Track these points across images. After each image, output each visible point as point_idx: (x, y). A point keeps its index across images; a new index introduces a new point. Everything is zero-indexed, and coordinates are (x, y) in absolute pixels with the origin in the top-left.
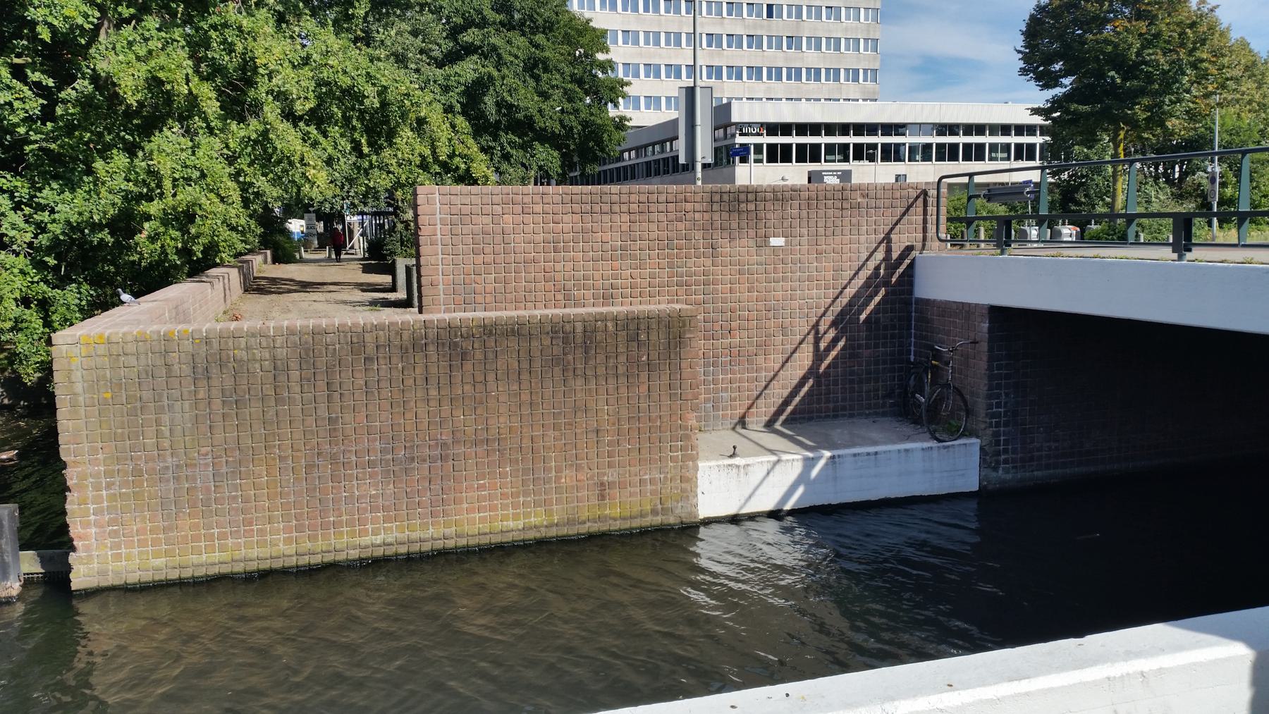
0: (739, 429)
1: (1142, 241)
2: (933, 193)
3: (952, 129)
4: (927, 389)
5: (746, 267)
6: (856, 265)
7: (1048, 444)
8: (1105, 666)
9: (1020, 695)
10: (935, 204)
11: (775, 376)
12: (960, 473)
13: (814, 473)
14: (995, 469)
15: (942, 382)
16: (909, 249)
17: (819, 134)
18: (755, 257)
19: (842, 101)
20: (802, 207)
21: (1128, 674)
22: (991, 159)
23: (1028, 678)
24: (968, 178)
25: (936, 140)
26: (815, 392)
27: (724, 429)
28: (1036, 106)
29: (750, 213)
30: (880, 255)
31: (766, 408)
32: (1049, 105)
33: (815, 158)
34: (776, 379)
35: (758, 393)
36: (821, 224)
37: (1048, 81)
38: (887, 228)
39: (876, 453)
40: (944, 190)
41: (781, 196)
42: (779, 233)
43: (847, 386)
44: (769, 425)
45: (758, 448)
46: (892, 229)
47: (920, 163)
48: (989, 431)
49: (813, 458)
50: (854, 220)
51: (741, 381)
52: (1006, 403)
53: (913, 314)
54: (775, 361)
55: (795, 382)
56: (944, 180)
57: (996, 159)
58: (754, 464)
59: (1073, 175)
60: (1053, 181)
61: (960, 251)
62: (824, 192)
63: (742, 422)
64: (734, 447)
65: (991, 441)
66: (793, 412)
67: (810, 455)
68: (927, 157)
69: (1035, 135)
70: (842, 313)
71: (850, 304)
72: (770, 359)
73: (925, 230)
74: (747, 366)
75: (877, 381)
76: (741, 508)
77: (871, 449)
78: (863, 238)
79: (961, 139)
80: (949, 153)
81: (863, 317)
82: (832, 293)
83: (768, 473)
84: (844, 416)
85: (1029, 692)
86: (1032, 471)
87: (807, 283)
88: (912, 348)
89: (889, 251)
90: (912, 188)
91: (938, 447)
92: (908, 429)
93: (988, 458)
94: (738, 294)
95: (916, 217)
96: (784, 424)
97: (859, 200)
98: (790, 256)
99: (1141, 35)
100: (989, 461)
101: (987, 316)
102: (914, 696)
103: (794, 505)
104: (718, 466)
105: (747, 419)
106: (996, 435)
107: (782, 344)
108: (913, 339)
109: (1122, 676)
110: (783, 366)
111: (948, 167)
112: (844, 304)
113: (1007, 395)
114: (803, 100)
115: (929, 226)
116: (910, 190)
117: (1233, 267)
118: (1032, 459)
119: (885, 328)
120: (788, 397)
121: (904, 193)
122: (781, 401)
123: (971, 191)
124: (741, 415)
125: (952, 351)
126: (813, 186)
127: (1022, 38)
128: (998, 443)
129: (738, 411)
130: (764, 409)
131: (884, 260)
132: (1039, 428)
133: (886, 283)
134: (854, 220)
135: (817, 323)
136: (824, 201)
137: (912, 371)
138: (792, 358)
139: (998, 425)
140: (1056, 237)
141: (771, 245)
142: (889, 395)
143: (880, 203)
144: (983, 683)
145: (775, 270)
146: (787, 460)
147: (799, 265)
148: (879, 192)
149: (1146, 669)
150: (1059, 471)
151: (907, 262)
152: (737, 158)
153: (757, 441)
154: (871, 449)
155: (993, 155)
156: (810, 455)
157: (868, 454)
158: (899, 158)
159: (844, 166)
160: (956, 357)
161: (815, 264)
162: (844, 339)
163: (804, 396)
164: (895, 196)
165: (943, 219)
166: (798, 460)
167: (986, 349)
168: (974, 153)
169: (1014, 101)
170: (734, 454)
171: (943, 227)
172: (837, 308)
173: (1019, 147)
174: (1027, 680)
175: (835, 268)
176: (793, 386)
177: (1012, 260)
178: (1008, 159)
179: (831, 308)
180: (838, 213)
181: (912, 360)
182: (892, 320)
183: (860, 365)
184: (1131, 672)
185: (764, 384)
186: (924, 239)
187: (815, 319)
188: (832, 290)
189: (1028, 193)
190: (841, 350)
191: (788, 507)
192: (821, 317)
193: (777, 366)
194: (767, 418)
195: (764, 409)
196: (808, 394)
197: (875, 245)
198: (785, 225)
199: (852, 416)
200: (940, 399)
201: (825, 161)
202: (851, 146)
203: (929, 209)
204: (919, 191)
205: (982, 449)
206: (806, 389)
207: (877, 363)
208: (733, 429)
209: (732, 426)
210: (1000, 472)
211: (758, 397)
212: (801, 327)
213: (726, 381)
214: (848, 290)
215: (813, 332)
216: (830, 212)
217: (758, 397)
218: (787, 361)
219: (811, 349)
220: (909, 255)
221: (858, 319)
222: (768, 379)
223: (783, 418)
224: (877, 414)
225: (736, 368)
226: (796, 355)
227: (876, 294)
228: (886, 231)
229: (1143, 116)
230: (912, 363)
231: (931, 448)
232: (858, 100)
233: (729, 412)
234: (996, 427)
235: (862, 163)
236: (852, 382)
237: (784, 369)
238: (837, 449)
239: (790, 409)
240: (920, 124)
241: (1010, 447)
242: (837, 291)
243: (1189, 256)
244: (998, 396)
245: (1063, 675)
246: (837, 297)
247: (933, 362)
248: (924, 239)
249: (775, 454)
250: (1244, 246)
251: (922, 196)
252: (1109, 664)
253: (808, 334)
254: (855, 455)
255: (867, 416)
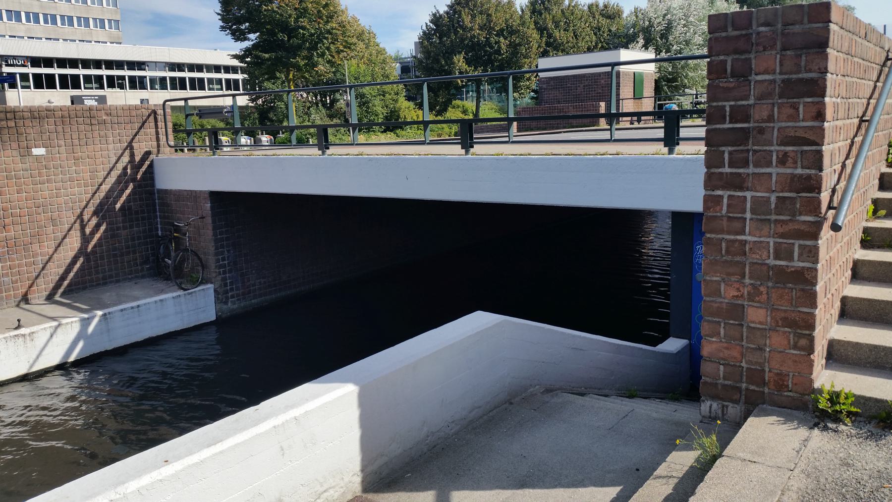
0: (23, 305)
1: (311, 143)
2: (160, 112)
3: (179, 67)
4: (173, 254)
5: (13, 173)
6: (108, 167)
7: (259, 281)
8: (272, 419)
9: (216, 454)
10: (163, 120)
11: (50, 259)
12: (202, 309)
13: (91, 329)
14: (226, 303)
15: (182, 247)
16: (148, 153)
17: (52, 67)
18: (20, 165)
19: (93, 43)
20: (58, 124)
21: (287, 421)
22: (210, 89)
23: (221, 441)
24: (183, 101)
25: (169, 74)
26: (86, 267)
27: (8, 307)
28: (234, 53)
29: (11, 129)
30: (126, 159)
31: (45, 285)
32: (243, 53)
33: (76, 86)
34: (52, 260)
35: (37, 274)
36: (75, 136)
37: (239, 36)
38: (129, 139)
39: (138, 306)
40: (168, 110)
41: (37, 115)
42: (39, 144)
43: (112, 259)
44: (50, 298)
45: (41, 318)
46: (133, 139)
47: (159, 91)
48: (219, 278)
49: (88, 318)
50: (102, 133)
51: (19, 266)
52: (228, 257)
53: (157, 201)
54: (48, 247)
55: (68, 261)
56: (167, 103)
57: (213, 89)
58: (37, 332)
59: (265, 101)
60: (252, 105)
61: (193, 154)
62: (74, 112)
63: (25, 299)
64: (19, 321)
65: (221, 284)
66: (69, 285)
67: (86, 316)
68: (163, 87)
69: (238, 73)
70: (101, 205)
71: (107, 197)
72: (44, 246)
73: (158, 139)
74: (24, 253)
75: (134, 252)
76: (31, 367)
77: (135, 304)
78: (111, 146)
79: (187, 75)
80: (180, 84)
81: (118, 206)
82: (91, 190)
83: (52, 336)
84: (111, 282)
85: (223, 450)
86: (251, 300)
87: (69, 183)
88: (159, 226)
89: (132, 155)
90: (145, 108)
91: (185, 294)
92: (161, 285)
93: (220, 296)
94: (8, 196)
95: (150, 129)
96: (63, 295)
97: (104, 118)
98: (52, 162)
99: (296, 9)
100: (221, 298)
101: (209, 198)
102: (140, 476)
103: (77, 357)
104: (4, 338)
105: (29, 296)
106: (224, 279)
107: (52, 235)
108: (159, 219)
109: (283, 423)
110: (56, 250)
111: (169, 94)
112: (101, 197)
113: (228, 251)
114: (61, 41)
115: (161, 136)
116: (143, 110)
117: (352, 158)
118: (249, 292)
119: (137, 213)
120: (63, 274)
121: (139, 112)
122: (57, 278)
123: (187, 111)
124: (23, 293)
125: (187, 225)
126: (78, 107)
127: (220, 5)
128: (226, 285)
129: (20, 291)
130: (44, 286)
131: (129, 162)
132: (252, 271)
133: (134, 180)
134: (102, 133)
135: (81, 214)
136: (76, 119)
137: (161, 242)
138: (64, 243)
139: (225, 272)
140: (257, 143)
141: (34, 154)
142: (146, 262)
143: (121, 120)
144: (190, 453)
145: (40, 175)
146: (67, 323)
147: (60, 169)
148: (119, 111)
149: (297, 415)
150: (268, 297)
151: (147, 163)
152: (6, 85)
153: (24, 311)
154: (135, 304)
155: (211, 86)
156: (86, 316)
157: (132, 308)
158: (143, 87)
159: (100, 92)
160: (191, 229)
161: (74, 168)
162: (105, 224)
163: (77, 272)
164: (132, 115)
165: (170, 131)
166: (76, 322)
167: (210, 221)
168: (197, 84)
169: (221, 49)
170: (19, 326)
171: (171, 137)
172: (97, 200)
173: (228, 81)
174: (220, 443)
175: (91, 170)
176: (67, 264)
177: (220, 159)
178: (222, 89)
179: (92, 201)
180: (89, 128)
181: (160, 235)
182: (141, 207)
183: (120, 242)
184: (288, 419)
185: (41, 266)
186: (158, 146)
187: (79, 211)
188: (90, 187)
189: (226, 112)
190: (104, 232)
191: (72, 359)
192: (84, 208)
193: (51, 251)
194: (47, 293)
195: (44, 286)
196: (80, 269)
197: (121, 152)
198: (44, 137)
199: (118, 281)
200: (182, 261)
201: (85, 88)
202: (105, 78)
203: (159, 124)
204: (150, 111)
205: (215, 291)
206: (78, 265)
207: (133, 239)
208: (18, 306)
209: (16, 303)
210: (229, 304)
211: (37, 277)
212: (69, 218)
213: (6, 268)
214: (103, 186)
215: (78, 221)
216: (82, 127)
217: (37, 277)
218: (59, 245)
219: (79, 234)
220: (148, 158)
221: (115, 207)
222: (44, 262)
223: (61, 291)
224: (137, 277)
225: (15, 256)
226: (67, 240)
227: (126, 188)
228: (129, 140)
229: (302, 63)
230: (160, 237)
231: (179, 295)
232: (106, 43)
233: (12, 293)
234: (223, 274)
235: (114, 90)
236: (115, 256)
237: (57, 252)
238: (107, 308)
239: (66, 283)
240: (156, 62)
241: (234, 286)
242: (95, 188)
243: (328, 152)
244: (222, 253)
245: (245, 433)
246: (95, 193)
247: (175, 234)
248: (158, 146)
249: (56, 320)
250: (357, 144)
251: (153, 115)
252: (275, 418)
253: (75, 222)
254: (122, 310)
255: (130, 280)
